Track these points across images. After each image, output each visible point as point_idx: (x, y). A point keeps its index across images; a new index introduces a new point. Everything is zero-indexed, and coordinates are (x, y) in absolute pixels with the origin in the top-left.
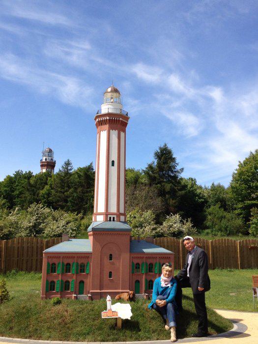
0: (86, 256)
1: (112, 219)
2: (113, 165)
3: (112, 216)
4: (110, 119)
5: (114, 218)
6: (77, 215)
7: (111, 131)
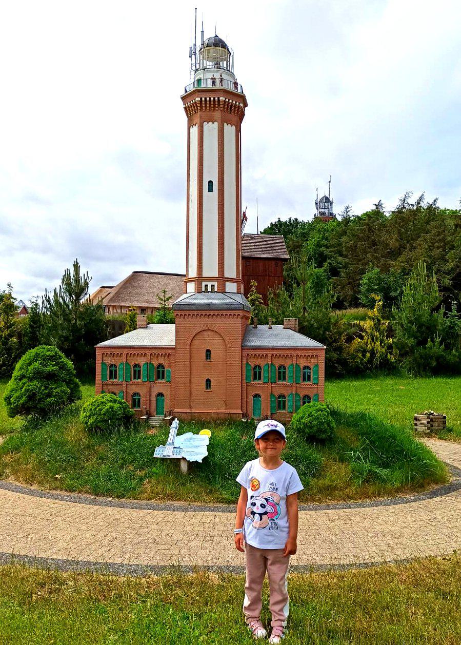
2: (210, 189)
3: (210, 284)
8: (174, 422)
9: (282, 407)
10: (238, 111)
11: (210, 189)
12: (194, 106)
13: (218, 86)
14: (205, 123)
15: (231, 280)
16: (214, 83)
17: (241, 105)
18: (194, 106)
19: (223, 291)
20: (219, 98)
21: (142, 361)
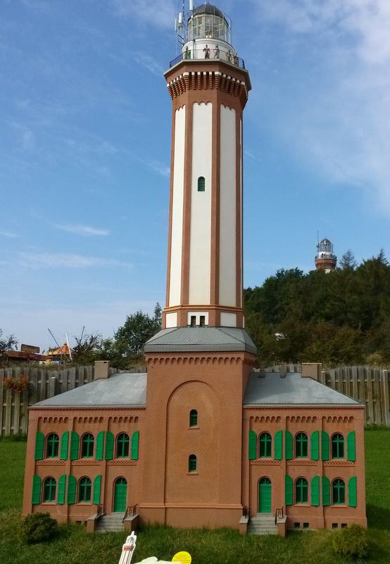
0: (128, 414)
1: (198, 322)
2: (201, 187)
3: (198, 315)
4: (221, 78)
5: (202, 318)
6: (341, 263)
7: (222, 107)
8: (129, 537)
9: (302, 453)
10: (239, 92)
11: (201, 187)
12: (180, 83)
13: (212, 57)
14: (196, 105)
15: (228, 310)
16: (207, 56)
17: (243, 83)
18: (180, 83)
19: (217, 325)
20: (213, 73)
21: (96, 430)
